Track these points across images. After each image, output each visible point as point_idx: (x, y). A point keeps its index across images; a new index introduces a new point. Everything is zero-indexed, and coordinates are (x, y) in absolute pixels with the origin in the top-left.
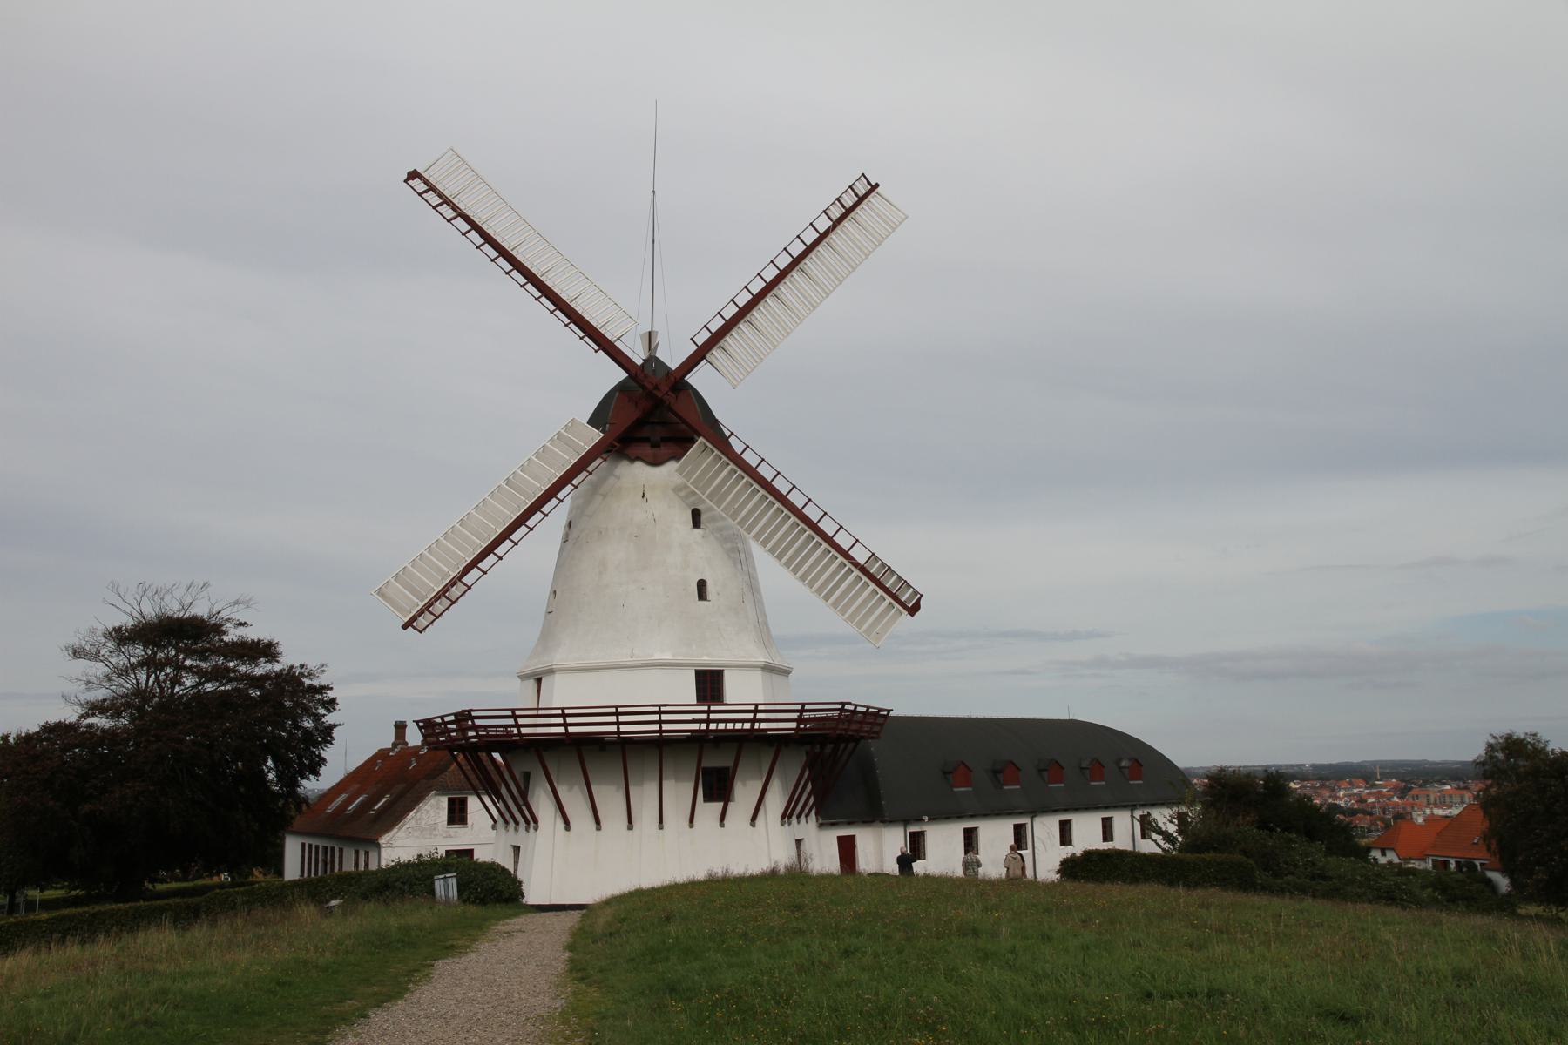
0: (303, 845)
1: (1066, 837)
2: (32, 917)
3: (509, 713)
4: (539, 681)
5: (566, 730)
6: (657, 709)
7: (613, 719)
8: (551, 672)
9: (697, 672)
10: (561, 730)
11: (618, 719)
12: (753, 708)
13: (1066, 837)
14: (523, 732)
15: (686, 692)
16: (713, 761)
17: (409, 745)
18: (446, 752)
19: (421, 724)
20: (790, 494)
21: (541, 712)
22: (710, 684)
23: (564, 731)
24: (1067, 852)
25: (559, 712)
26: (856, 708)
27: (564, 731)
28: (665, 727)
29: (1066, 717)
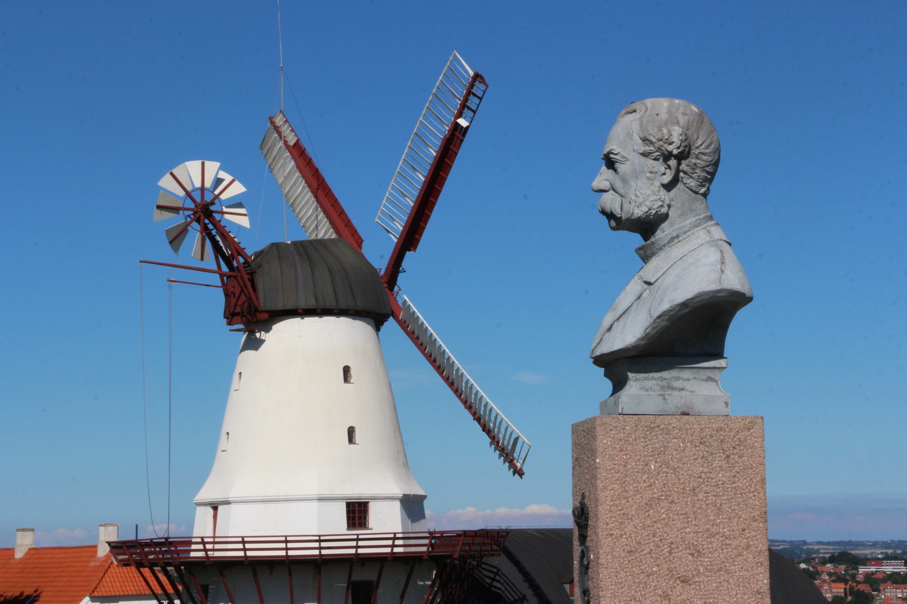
4: (215, 508)
5: (245, 553)
8: (227, 503)
10: (241, 554)
12: (392, 536)
14: (204, 553)
16: (360, 575)
17: (87, 599)
18: (133, 568)
19: (112, 545)
20: (138, 536)
25: (240, 539)
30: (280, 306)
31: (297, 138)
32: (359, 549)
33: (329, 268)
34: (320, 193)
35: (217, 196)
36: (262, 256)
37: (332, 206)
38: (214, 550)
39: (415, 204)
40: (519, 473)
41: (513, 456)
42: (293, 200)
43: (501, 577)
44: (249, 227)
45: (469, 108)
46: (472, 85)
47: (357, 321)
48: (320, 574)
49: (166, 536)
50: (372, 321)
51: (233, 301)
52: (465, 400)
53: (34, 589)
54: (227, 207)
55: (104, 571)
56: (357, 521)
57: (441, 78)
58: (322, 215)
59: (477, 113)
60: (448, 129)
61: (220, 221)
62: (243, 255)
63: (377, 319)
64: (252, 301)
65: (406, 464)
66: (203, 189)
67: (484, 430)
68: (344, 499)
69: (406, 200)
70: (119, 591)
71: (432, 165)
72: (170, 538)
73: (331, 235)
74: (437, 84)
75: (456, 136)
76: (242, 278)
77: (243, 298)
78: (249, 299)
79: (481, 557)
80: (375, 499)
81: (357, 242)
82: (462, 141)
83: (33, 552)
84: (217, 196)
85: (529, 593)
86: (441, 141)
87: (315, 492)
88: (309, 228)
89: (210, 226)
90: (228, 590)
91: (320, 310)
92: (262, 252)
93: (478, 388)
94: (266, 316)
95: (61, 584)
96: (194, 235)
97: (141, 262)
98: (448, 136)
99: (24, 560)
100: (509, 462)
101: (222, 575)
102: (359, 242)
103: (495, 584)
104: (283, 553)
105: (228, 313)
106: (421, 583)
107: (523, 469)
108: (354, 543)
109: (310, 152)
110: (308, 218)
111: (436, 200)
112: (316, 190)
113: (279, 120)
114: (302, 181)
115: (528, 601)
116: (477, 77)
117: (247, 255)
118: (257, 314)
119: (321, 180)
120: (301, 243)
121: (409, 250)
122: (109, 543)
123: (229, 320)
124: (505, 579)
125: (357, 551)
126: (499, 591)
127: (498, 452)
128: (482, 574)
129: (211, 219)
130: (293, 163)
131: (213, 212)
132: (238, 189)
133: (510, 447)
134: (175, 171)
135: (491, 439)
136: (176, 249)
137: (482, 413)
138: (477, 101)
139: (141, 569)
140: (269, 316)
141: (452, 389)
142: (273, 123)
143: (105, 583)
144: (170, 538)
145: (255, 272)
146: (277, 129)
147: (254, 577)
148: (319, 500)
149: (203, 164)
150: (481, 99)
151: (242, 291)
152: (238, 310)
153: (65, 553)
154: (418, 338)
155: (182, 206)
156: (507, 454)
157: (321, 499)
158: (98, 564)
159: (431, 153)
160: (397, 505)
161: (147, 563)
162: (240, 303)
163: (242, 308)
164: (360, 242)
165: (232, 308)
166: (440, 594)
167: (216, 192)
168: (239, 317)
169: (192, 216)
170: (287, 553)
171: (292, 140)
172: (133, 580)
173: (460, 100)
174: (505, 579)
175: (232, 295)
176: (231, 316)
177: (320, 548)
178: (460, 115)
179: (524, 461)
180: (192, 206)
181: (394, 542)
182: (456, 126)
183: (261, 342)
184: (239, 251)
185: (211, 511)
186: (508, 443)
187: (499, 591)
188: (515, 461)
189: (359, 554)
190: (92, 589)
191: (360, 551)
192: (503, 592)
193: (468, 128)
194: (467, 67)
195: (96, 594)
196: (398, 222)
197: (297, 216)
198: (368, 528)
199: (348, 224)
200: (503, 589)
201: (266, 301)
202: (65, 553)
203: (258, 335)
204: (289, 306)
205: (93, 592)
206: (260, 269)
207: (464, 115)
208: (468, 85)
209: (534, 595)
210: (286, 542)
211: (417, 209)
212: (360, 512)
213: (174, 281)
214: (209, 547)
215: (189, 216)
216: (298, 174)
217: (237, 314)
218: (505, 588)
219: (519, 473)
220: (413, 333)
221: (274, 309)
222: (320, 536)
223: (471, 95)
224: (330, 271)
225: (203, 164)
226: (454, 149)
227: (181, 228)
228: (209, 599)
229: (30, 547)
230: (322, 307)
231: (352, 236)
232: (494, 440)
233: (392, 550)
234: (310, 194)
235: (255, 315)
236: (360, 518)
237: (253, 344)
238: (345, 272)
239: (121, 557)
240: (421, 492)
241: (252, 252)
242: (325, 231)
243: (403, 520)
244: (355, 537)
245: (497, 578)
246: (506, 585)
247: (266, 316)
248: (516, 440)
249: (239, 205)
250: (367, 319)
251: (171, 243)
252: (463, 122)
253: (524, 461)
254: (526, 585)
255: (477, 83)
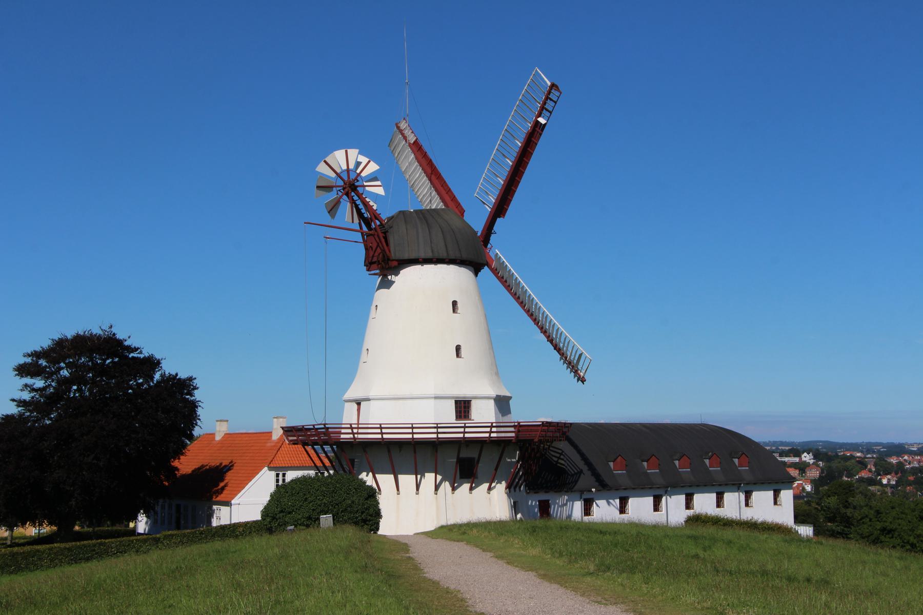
0: (278, 475)
1: (689, 505)
2: (892, 460)
3: (349, 426)
4: (359, 404)
5: (382, 436)
6: (436, 425)
7: (410, 431)
8: (368, 400)
9: (456, 402)
10: (379, 436)
11: (413, 430)
12: (490, 425)
13: (689, 505)
15: (448, 414)
16: (466, 453)
17: (266, 468)
18: (300, 446)
21: (343, 426)
22: (463, 408)
23: (381, 437)
24: (690, 512)
25: (379, 426)
26: (465, 425)
27: (381, 437)
28: (440, 436)
29: (609, 422)
30: (406, 257)
31: (415, 138)
32: (466, 434)
33: (441, 229)
34: (433, 177)
35: (359, 174)
36: (392, 220)
37: (442, 186)
38: (358, 433)
39: (522, 145)
40: (583, 380)
41: (577, 368)
42: (413, 182)
43: (564, 456)
44: (384, 194)
45: (547, 110)
46: (549, 93)
47: (462, 268)
48: (437, 451)
49: (324, 422)
50: (473, 269)
51: (371, 253)
52: (541, 326)
53: (230, 461)
54: (365, 182)
55: (277, 449)
56: (463, 414)
57: (525, 88)
58: (434, 193)
59: (553, 113)
60: (530, 125)
61: (362, 194)
62: (379, 219)
63: (476, 266)
64: (385, 252)
65: (497, 374)
66: (348, 170)
67: (555, 349)
68: (453, 398)
69: (489, 198)
70: (288, 464)
71: (509, 172)
72: (327, 424)
73: (441, 206)
74: (523, 93)
75: (537, 129)
76: (378, 236)
77: (379, 250)
78: (383, 251)
79: (552, 442)
80: (476, 398)
81: (460, 212)
82: (541, 134)
83: (228, 436)
84: (359, 174)
85: (585, 468)
86: (525, 135)
87: (432, 392)
88: (425, 202)
89: (356, 198)
90: (369, 463)
91: (435, 260)
92: (392, 217)
93: (552, 317)
94: (396, 263)
95: (247, 458)
96: (346, 207)
97: (305, 223)
98: (530, 131)
99: (221, 442)
100: (574, 373)
101: (365, 451)
102: (462, 212)
103: (560, 461)
104: (410, 436)
105: (367, 262)
106: (509, 460)
107: (585, 377)
108: (462, 430)
109: (426, 147)
110: (424, 195)
111: (521, 179)
112: (430, 175)
113: (403, 125)
114: (419, 169)
115: (584, 474)
116: (553, 86)
117: (382, 219)
118: (389, 262)
119: (434, 168)
120: (421, 211)
121: (500, 217)
122: (283, 428)
123: (368, 267)
124: (568, 458)
125: (464, 435)
126: (563, 466)
127: (565, 365)
128: (550, 454)
129: (356, 192)
130: (413, 156)
131: (357, 186)
132: (373, 167)
133: (575, 362)
134: (327, 159)
135: (560, 355)
136: (333, 216)
137: (554, 336)
138: (552, 104)
139: (306, 447)
140: (399, 264)
141: (532, 319)
142: (398, 128)
143: (278, 458)
144: (327, 424)
145: (387, 231)
146: (401, 132)
147: (389, 455)
148: (435, 398)
149: (346, 151)
150: (555, 102)
151: (378, 245)
152: (375, 259)
153: (250, 437)
154: (506, 281)
155: (335, 185)
156: (573, 367)
157: (436, 398)
158: (273, 444)
159: (545, 82)
160: (492, 402)
161: (310, 442)
162: (376, 254)
163: (378, 258)
164: (462, 211)
165: (370, 259)
166: (522, 469)
167: (358, 171)
168: (376, 265)
169: (342, 191)
170: (413, 436)
171: (412, 139)
172: (297, 456)
173: (540, 103)
174: (568, 458)
175: (371, 249)
176: (370, 264)
177: (438, 433)
178: (539, 115)
179: (586, 371)
180: (342, 183)
181: (491, 429)
182: (537, 123)
183: (392, 283)
184: (376, 216)
185: (356, 406)
186: (574, 359)
187: (563, 466)
188: (579, 371)
189: (466, 438)
190: (269, 461)
191: (467, 435)
192: (566, 467)
193: (545, 124)
194: (546, 79)
195: (272, 465)
196: (500, 178)
197: (416, 194)
198: (470, 420)
199: (454, 199)
200: (566, 465)
201: (396, 252)
202: (250, 437)
203: (389, 277)
204: (413, 256)
205: (270, 463)
206: (392, 229)
207: (543, 115)
208: (546, 93)
209: (589, 470)
210: (413, 428)
211: (506, 187)
212: (465, 407)
213: (328, 238)
214: (355, 431)
215: (339, 190)
216: (417, 163)
217: (374, 263)
218: (568, 464)
219: (583, 380)
220: (503, 278)
221: (402, 258)
222: (437, 424)
223: (549, 100)
224: (442, 231)
225: (346, 151)
226: (534, 141)
227: (334, 203)
228: (355, 469)
229: (226, 432)
230: (436, 257)
231: (457, 208)
232: (562, 355)
233: (490, 435)
234: (425, 177)
235: (388, 263)
236: (465, 412)
237: (386, 284)
238: (453, 232)
239: (291, 438)
240: (508, 394)
241: (386, 217)
242: (436, 203)
243: (496, 414)
244: (463, 425)
245: (562, 457)
246: (568, 462)
247: (396, 263)
248: (580, 355)
249: (375, 179)
250: (470, 267)
251: (329, 212)
252: (542, 120)
253: (586, 371)
254: (583, 462)
255: (553, 91)
